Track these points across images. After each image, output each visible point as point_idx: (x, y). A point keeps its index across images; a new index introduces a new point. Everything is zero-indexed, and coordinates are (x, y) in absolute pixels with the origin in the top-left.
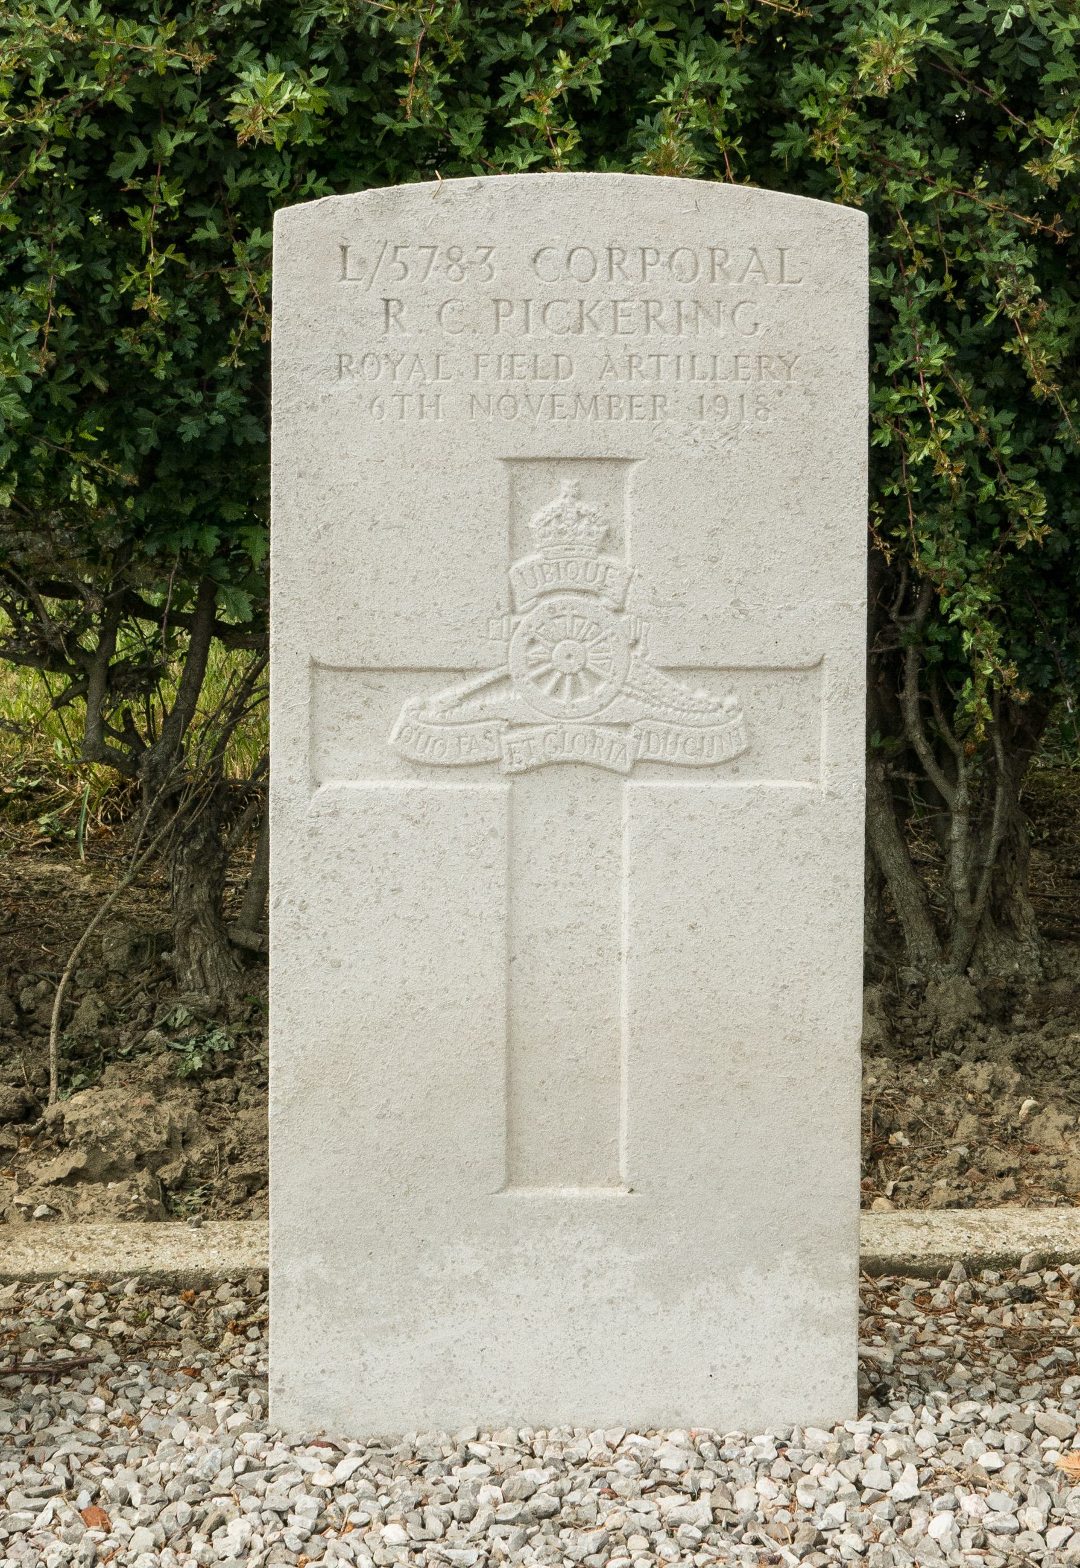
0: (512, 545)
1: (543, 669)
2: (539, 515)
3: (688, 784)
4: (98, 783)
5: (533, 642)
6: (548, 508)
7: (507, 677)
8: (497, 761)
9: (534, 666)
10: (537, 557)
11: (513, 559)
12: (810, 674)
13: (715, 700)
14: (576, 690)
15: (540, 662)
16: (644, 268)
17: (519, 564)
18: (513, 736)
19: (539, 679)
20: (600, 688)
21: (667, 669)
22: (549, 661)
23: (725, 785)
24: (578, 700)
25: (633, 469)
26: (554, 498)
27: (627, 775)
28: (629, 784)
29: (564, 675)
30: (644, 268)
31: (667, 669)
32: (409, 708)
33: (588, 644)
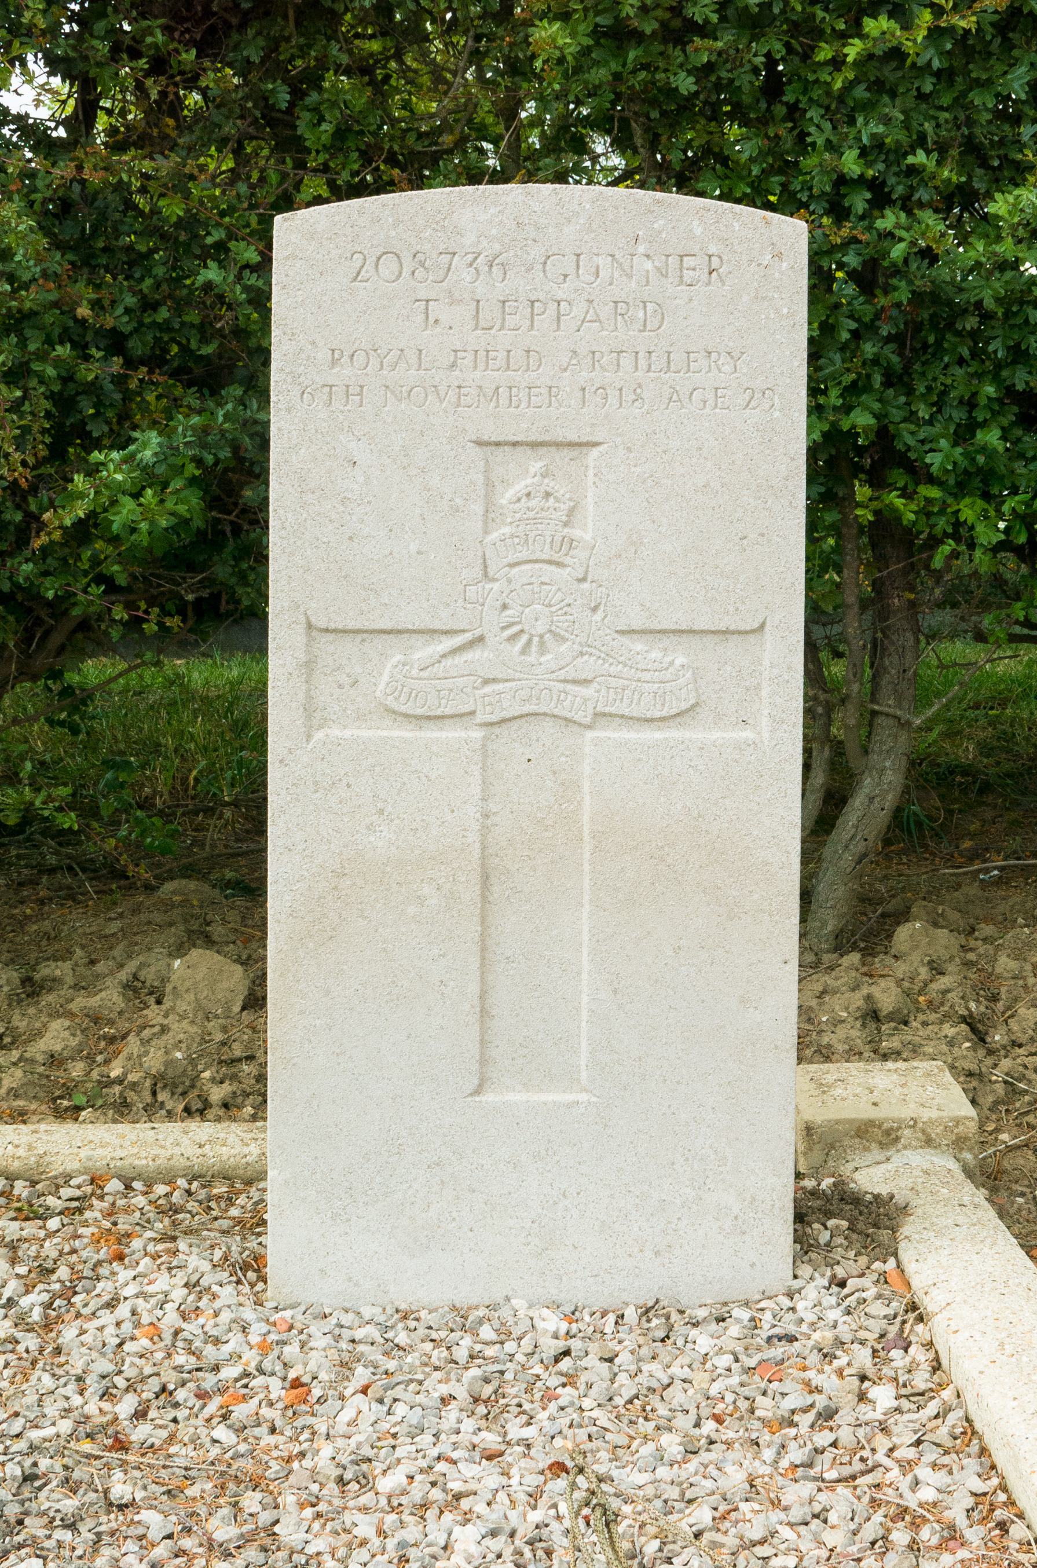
0: (485, 523)
1: (515, 629)
2: (510, 493)
3: (658, 735)
4: (72, 30)
5: (505, 607)
6: (517, 487)
7: (481, 639)
8: (473, 713)
9: (504, 628)
10: (507, 530)
11: (486, 532)
12: (752, 638)
13: (668, 659)
14: (543, 649)
15: (513, 624)
16: (558, 318)
17: (494, 536)
18: (488, 689)
19: (513, 638)
20: (564, 647)
21: (622, 632)
22: (520, 623)
23: (673, 733)
24: (543, 659)
25: (595, 452)
26: (524, 475)
27: (589, 727)
28: (590, 734)
29: (541, 636)
30: (558, 318)
31: (622, 632)
32: (388, 669)
33: (553, 609)
